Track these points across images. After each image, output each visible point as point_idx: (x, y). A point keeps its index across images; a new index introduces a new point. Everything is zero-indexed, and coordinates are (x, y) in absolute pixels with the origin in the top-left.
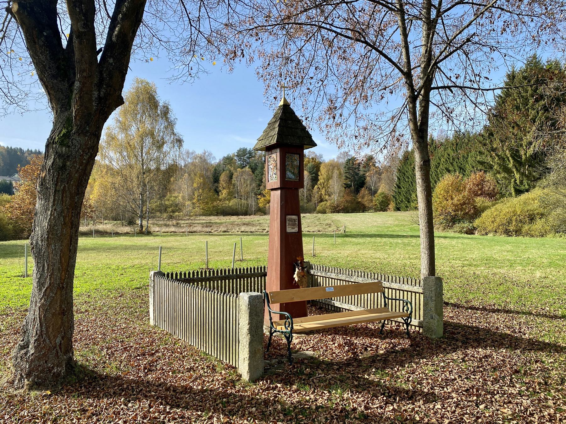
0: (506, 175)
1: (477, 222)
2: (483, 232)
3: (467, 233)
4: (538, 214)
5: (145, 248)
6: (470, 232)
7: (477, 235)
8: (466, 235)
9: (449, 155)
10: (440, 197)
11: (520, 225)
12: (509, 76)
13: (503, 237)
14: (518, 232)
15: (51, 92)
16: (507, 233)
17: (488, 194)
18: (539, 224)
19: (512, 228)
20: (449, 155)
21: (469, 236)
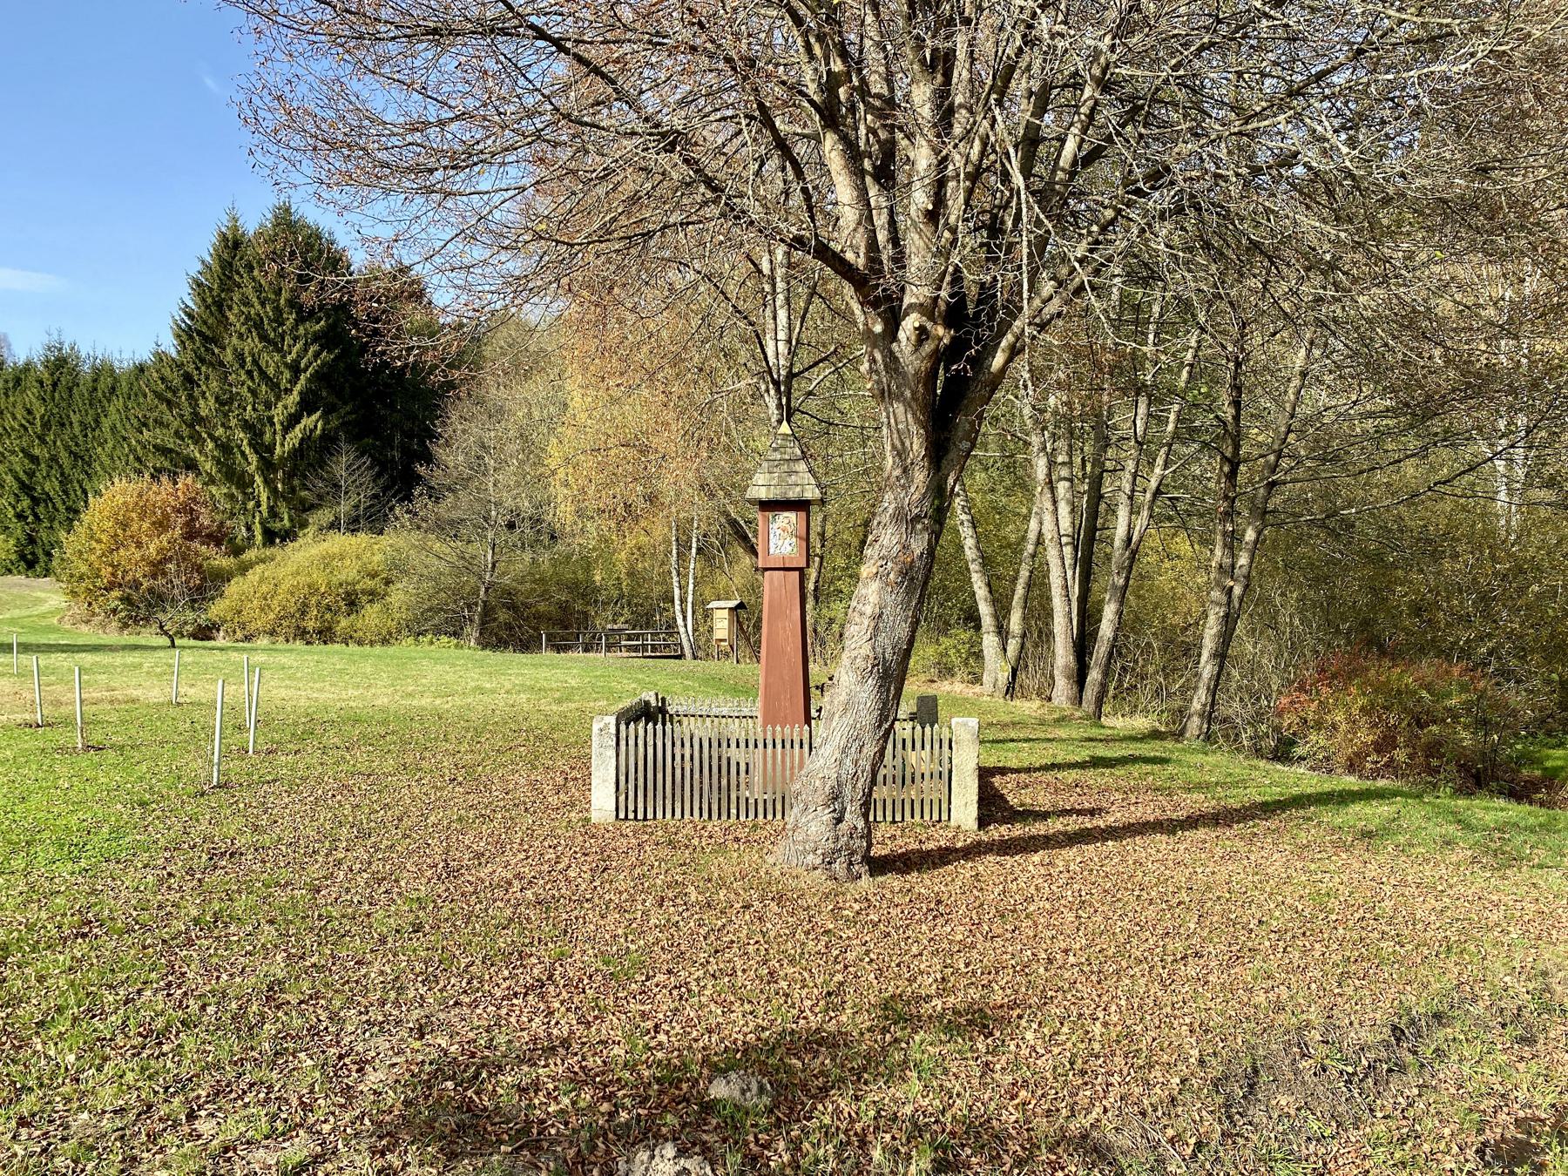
0: (234, 490)
1: (217, 609)
2: (239, 635)
3: (194, 636)
4: (364, 592)
5: (205, 648)
6: (204, 633)
7: (221, 641)
8: (192, 642)
9: (30, 412)
10: (104, 537)
11: (328, 616)
12: (224, 237)
13: (299, 645)
14: (326, 634)
15: (240, 342)
16: (302, 634)
17: (210, 536)
18: (371, 615)
19: (311, 625)
20: (30, 412)
21: (200, 643)
